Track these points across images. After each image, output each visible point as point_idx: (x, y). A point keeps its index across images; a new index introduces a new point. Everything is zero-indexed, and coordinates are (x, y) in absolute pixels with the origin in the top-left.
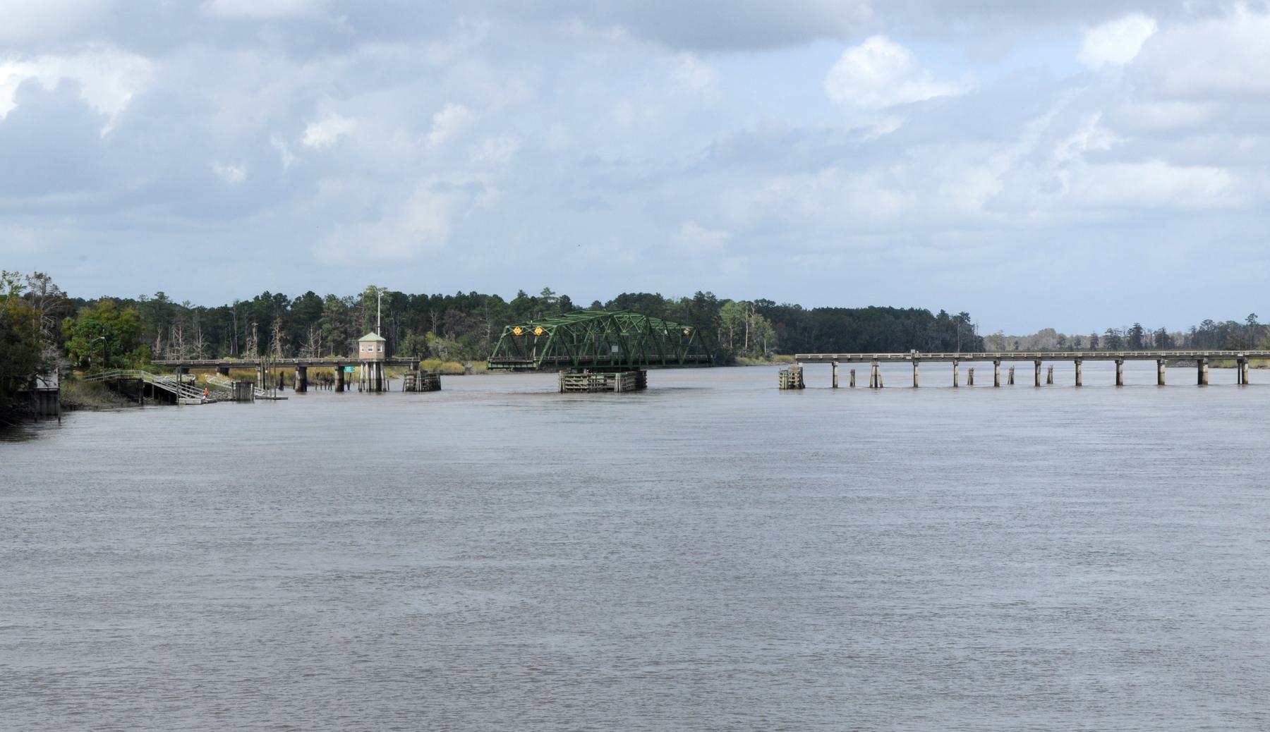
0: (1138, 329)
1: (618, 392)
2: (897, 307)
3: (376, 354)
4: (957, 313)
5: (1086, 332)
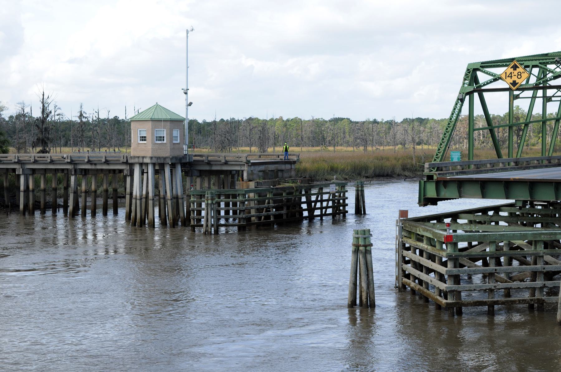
3: (150, 147)
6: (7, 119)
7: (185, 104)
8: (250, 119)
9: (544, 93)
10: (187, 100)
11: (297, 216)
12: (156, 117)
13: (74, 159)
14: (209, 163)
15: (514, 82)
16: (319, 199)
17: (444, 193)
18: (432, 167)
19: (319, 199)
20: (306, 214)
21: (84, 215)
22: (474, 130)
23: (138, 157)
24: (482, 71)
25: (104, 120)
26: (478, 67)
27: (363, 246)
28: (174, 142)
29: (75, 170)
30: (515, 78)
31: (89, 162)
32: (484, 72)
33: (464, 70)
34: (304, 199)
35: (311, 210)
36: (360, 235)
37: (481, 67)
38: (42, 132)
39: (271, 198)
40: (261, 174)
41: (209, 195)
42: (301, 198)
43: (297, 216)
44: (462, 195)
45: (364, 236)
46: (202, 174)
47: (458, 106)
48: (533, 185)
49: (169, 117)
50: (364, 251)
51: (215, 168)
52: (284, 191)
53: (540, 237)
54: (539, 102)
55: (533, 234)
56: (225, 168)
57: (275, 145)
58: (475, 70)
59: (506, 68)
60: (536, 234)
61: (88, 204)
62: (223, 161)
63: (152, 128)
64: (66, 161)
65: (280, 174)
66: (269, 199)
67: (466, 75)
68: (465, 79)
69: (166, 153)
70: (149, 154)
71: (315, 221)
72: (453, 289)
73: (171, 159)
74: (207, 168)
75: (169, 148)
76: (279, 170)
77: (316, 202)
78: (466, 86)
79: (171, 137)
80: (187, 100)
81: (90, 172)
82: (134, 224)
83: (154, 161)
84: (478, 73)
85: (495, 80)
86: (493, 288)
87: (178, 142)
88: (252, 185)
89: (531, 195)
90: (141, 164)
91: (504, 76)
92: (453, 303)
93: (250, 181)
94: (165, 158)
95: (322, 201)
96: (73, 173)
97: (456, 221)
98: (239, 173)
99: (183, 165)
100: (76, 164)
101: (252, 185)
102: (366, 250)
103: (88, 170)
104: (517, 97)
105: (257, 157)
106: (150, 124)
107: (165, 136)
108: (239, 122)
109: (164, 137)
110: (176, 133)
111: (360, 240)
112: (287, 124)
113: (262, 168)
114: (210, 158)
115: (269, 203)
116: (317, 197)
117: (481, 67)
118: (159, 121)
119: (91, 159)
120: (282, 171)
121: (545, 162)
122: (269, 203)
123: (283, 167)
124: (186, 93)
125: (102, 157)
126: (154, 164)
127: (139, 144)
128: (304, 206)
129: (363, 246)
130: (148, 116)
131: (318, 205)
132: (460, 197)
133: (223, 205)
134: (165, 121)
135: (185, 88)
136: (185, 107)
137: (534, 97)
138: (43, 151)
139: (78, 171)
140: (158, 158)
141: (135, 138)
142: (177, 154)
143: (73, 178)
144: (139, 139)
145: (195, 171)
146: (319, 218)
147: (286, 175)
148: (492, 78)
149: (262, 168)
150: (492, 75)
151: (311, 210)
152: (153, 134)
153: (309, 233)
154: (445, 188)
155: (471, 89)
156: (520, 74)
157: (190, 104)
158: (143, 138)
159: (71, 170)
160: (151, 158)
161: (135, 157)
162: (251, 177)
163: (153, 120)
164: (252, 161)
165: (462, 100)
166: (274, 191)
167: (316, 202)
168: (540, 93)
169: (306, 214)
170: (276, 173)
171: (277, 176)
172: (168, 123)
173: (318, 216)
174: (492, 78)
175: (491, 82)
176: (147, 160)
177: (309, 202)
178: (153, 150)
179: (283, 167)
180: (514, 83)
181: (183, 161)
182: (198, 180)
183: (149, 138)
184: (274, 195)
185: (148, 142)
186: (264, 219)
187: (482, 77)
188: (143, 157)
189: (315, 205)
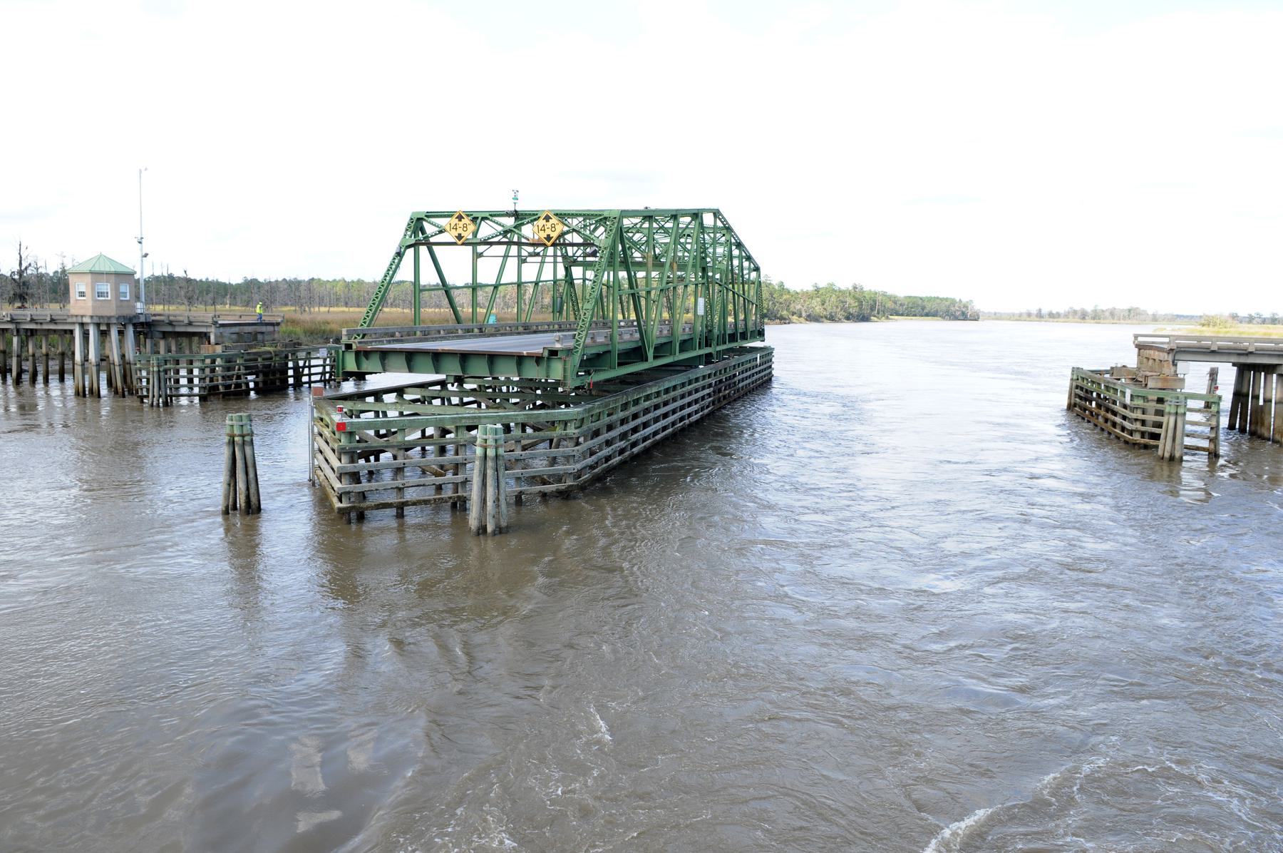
0: (1040, 310)
1: (482, 530)
2: (941, 297)
3: (90, 304)
4: (968, 300)
5: (1017, 311)
6: (51, 274)
7: (139, 255)
8: (313, 279)
9: (519, 251)
10: (141, 250)
11: (244, 388)
12: (97, 269)
13: (15, 318)
14: (171, 323)
15: (460, 235)
16: (307, 364)
17: (366, 366)
18: (349, 335)
19: (307, 364)
20: (291, 381)
21: (46, 381)
22: (421, 291)
23: (77, 316)
24: (427, 221)
25: (157, 277)
26: (423, 216)
27: (240, 436)
28: (122, 299)
29: (18, 331)
30: (460, 231)
31: (32, 320)
32: (429, 223)
33: (407, 220)
34: (291, 364)
35: (298, 376)
36: (234, 422)
37: (426, 216)
38: (20, 287)
39: (242, 364)
40: (234, 336)
41: (155, 362)
42: (287, 364)
43: (244, 388)
44: (387, 368)
45: (241, 423)
46: (165, 335)
47: (396, 261)
48: (464, 357)
49: (113, 270)
50: (240, 442)
51: (178, 329)
52: (260, 356)
53: (460, 421)
54: (512, 263)
55: (452, 418)
56: (190, 329)
57: (320, 305)
58: (420, 220)
59: (449, 219)
60: (455, 418)
61: (66, 367)
62: (186, 321)
63: (92, 282)
64: (6, 319)
65: (260, 337)
66: (239, 365)
67: (409, 224)
68: (407, 230)
69: (111, 311)
70: (90, 313)
71: (303, 389)
72: (348, 490)
73: (118, 318)
74: (169, 329)
75: (114, 306)
76: (257, 333)
77: (304, 367)
78: (407, 237)
79: (117, 293)
80: (141, 250)
81: (38, 333)
82: (116, 392)
83: (96, 320)
84: (424, 223)
85: (441, 232)
86: (401, 486)
87: (128, 298)
88: (219, 349)
89: (464, 369)
90: (82, 324)
91: (448, 228)
92: (348, 508)
93: (217, 344)
94: (109, 318)
95: (310, 367)
96: (15, 333)
97: (402, 396)
98: (205, 336)
99: (135, 325)
100: (19, 323)
101: (219, 349)
102: (244, 441)
103: (36, 330)
104: (481, 255)
105: (237, 318)
106: (89, 277)
107: (109, 291)
108: (300, 282)
109: (107, 293)
110: (125, 288)
111: (235, 427)
112: (348, 285)
113: (236, 329)
114: (171, 318)
115: (239, 370)
116: (305, 363)
117: (426, 216)
118: (101, 273)
119: (35, 318)
120: (263, 333)
121: (521, 329)
122: (239, 370)
123: (264, 329)
124: (140, 243)
125: (27, 316)
126: (98, 325)
127: (77, 300)
128: (291, 372)
129: (240, 436)
130: (86, 269)
131: (306, 371)
132: (385, 371)
133: (183, 372)
134: (107, 274)
135: (139, 238)
136: (140, 259)
137: (506, 256)
138: (22, 307)
139: (22, 332)
140: (100, 317)
141: (74, 294)
142: (126, 312)
143: (15, 340)
144: (77, 294)
145: (157, 333)
146: (307, 385)
147: (267, 338)
148: (438, 229)
149: (236, 329)
150: (438, 227)
151: (298, 376)
152: (93, 289)
153: (297, 399)
154: (367, 359)
155: (412, 241)
156: (465, 226)
157: (146, 255)
158: (82, 294)
159: (12, 330)
160: (92, 317)
161: (72, 316)
162: (220, 340)
163: (92, 273)
164: (220, 322)
165: (399, 255)
166: (246, 357)
167: (304, 367)
168: (514, 249)
169: (291, 381)
170: (254, 336)
171: (255, 339)
172: (113, 277)
173: (306, 383)
174: (438, 229)
175: (436, 234)
176: (86, 320)
177: (296, 368)
178: (94, 307)
179: (264, 329)
180: (460, 237)
181: (135, 321)
182: (162, 344)
183: (89, 294)
184: (246, 360)
185: (88, 297)
186: (235, 388)
187: (429, 229)
188: (82, 316)
189: (303, 371)
